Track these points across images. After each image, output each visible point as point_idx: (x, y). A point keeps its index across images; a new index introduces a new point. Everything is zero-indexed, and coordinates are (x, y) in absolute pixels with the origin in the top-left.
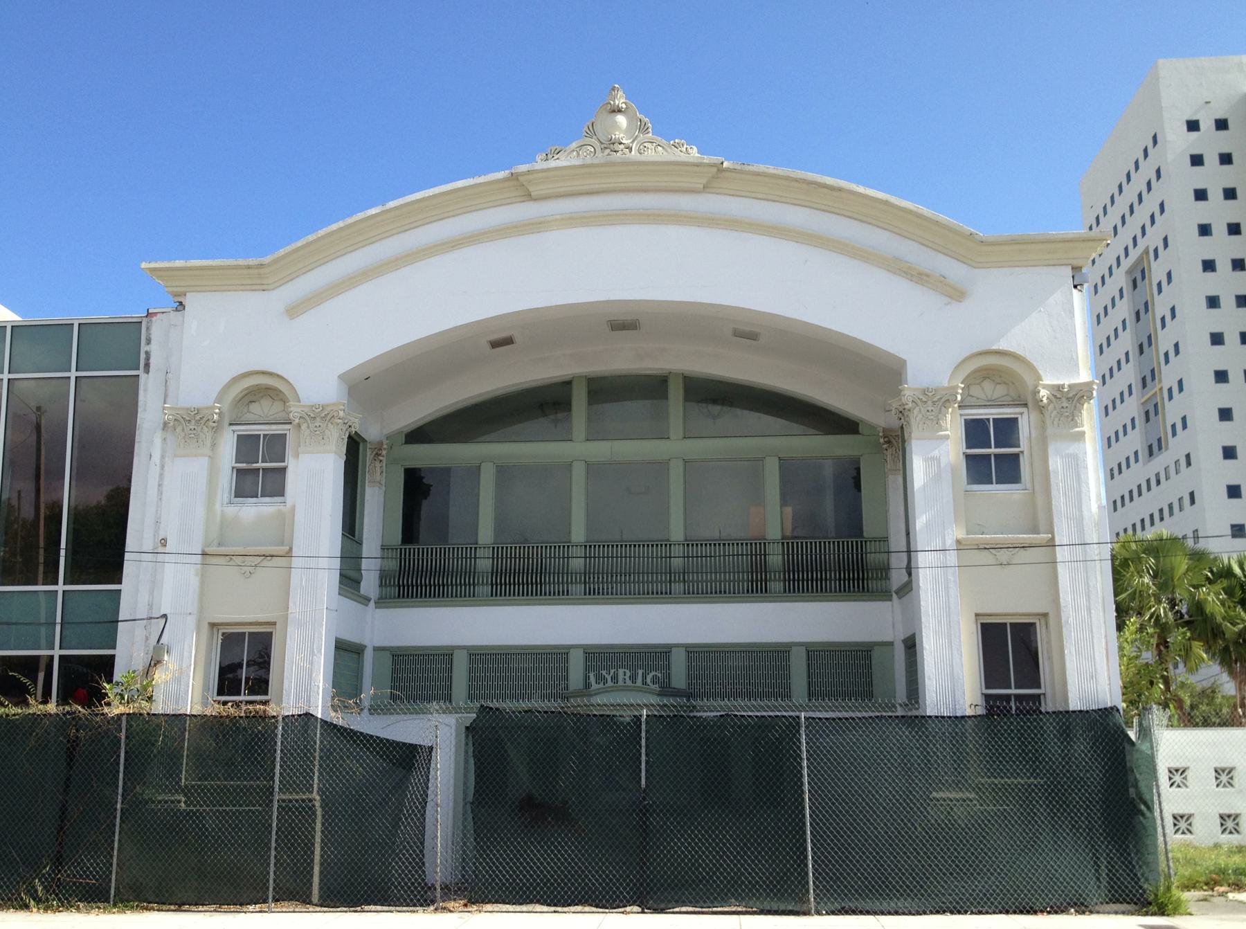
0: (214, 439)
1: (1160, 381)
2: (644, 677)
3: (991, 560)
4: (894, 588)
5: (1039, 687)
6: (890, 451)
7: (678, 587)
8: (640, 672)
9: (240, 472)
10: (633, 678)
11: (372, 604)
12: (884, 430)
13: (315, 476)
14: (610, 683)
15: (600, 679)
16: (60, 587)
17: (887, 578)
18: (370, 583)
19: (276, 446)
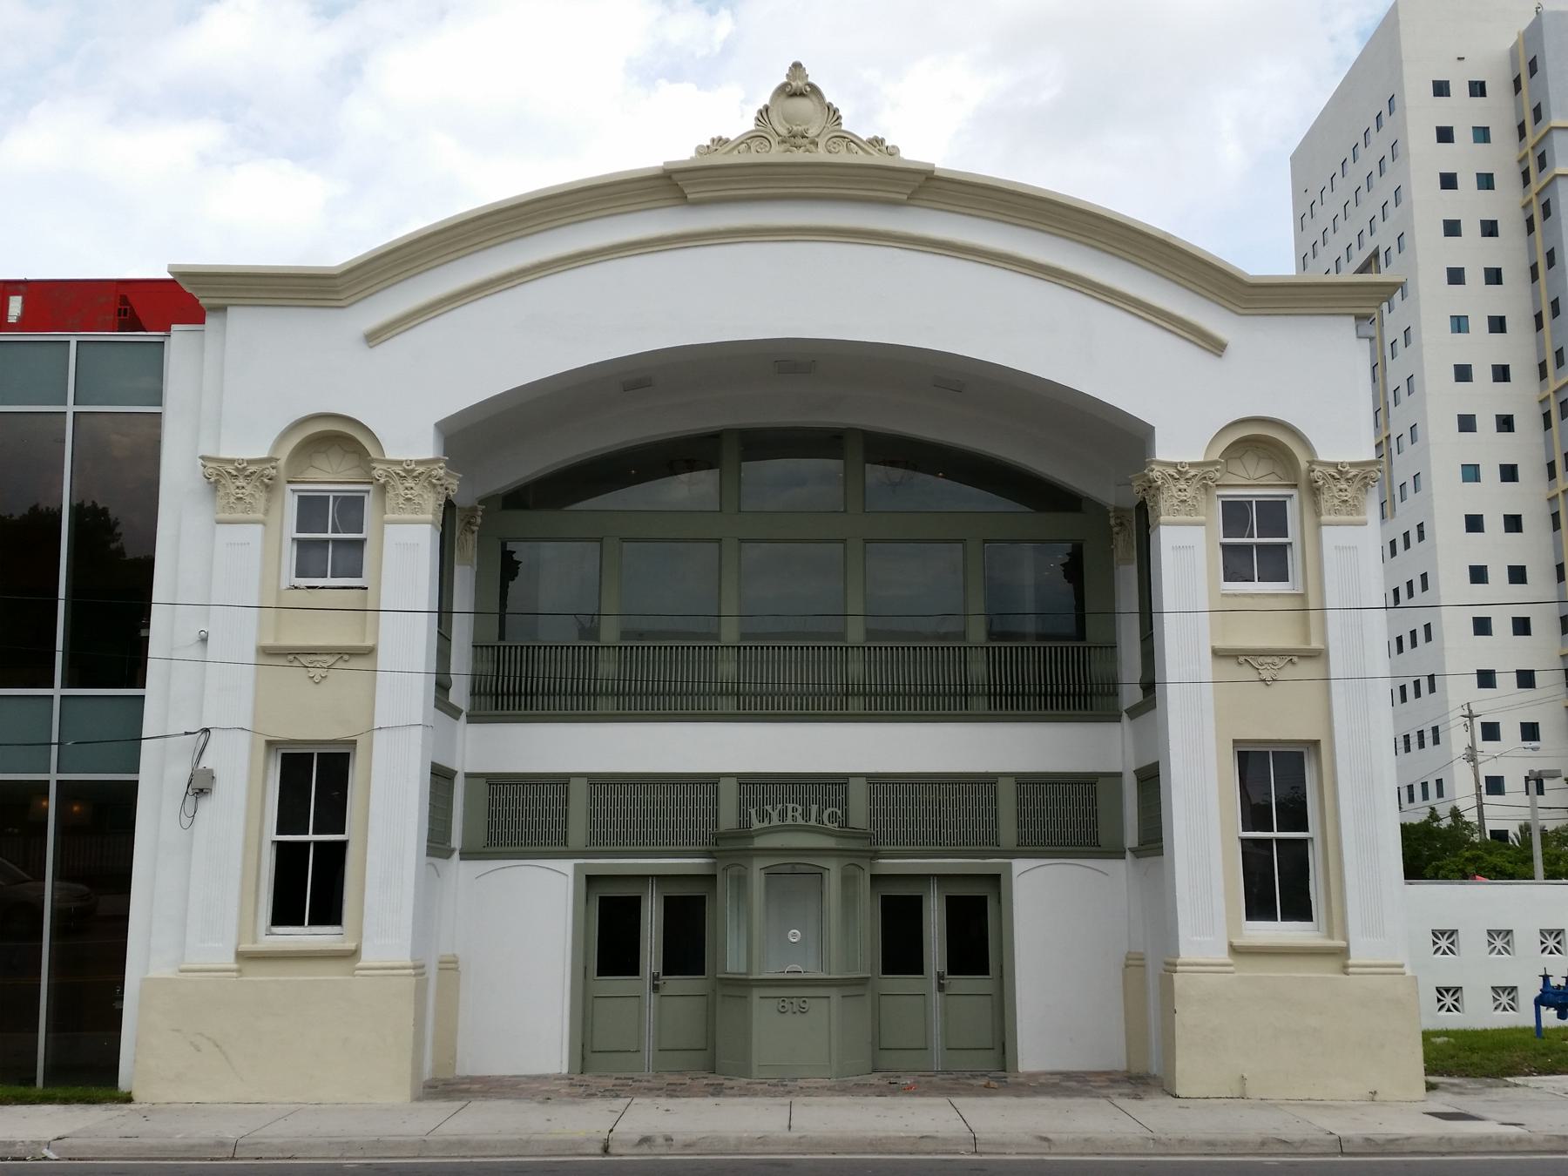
0: (268, 500)
1: (1387, 427)
2: (820, 813)
3: (1253, 675)
4: (1125, 707)
5: (1306, 830)
6: (1120, 538)
7: (856, 704)
8: (814, 808)
9: (302, 544)
10: (806, 815)
11: (463, 717)
12: (1116, 509)
13: (405, 552)
14: (776, 821)
15: (763, 815)
16: (57, 691)
17: (1115, 694)
18: (460, 694)
19: (351, 509)
